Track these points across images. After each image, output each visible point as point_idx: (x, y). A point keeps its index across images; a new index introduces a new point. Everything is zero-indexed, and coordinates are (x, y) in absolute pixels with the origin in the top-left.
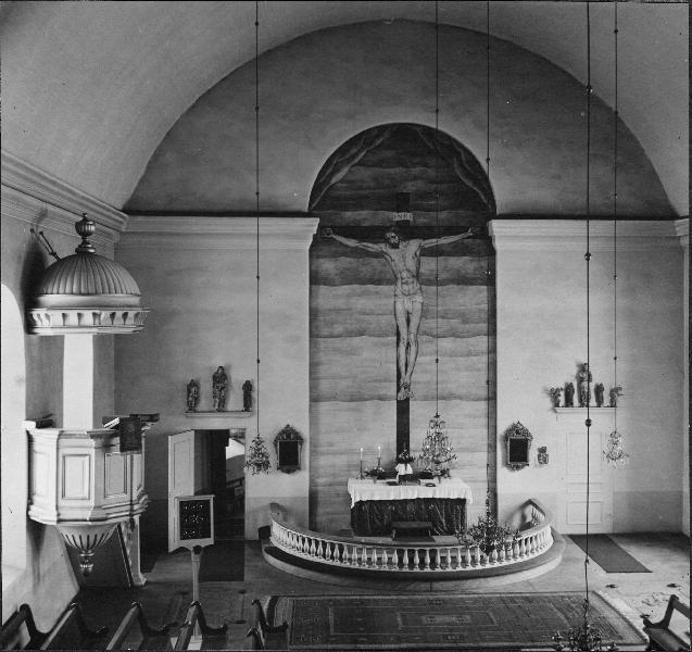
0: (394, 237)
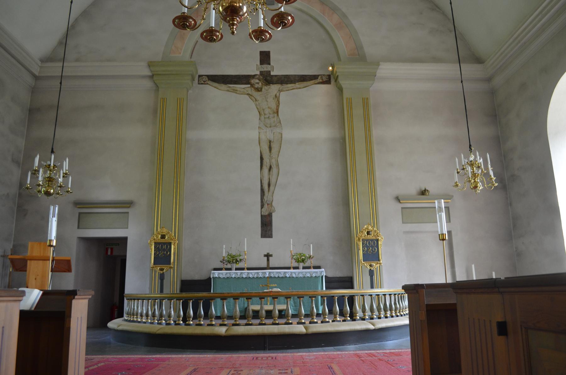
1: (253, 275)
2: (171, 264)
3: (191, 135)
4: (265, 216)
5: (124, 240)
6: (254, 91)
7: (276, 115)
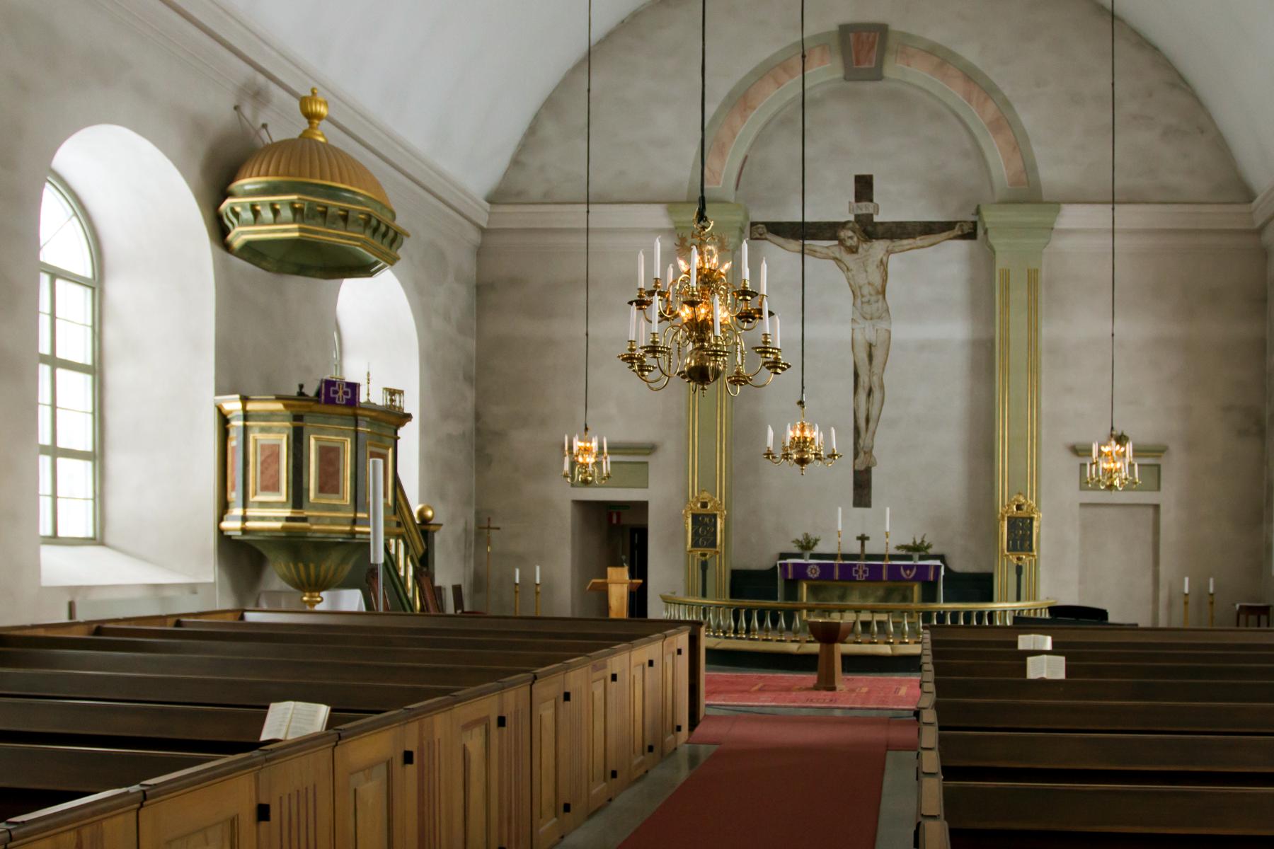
0: (851, 238)
7: (881, 297)
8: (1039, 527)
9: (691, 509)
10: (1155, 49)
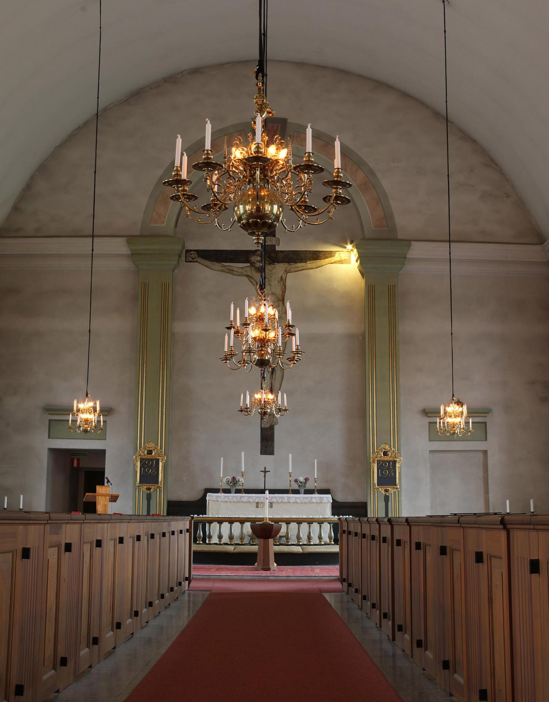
1: (254, 499)
2: (159, 483)
3: (179, 327)
4: (266, 429)
5: (102, 453)
6: (254, 271)
7: (281, 303)
8: (400, 468)
9: (140, 455)
10: (475, 141)
